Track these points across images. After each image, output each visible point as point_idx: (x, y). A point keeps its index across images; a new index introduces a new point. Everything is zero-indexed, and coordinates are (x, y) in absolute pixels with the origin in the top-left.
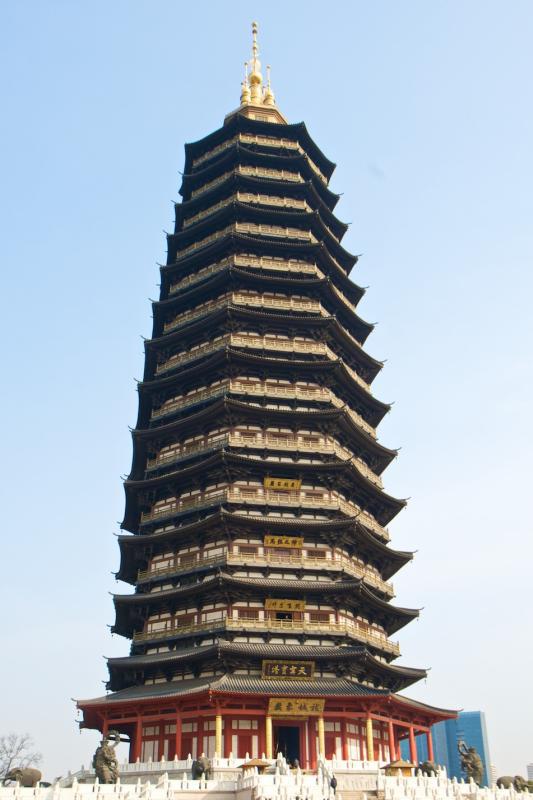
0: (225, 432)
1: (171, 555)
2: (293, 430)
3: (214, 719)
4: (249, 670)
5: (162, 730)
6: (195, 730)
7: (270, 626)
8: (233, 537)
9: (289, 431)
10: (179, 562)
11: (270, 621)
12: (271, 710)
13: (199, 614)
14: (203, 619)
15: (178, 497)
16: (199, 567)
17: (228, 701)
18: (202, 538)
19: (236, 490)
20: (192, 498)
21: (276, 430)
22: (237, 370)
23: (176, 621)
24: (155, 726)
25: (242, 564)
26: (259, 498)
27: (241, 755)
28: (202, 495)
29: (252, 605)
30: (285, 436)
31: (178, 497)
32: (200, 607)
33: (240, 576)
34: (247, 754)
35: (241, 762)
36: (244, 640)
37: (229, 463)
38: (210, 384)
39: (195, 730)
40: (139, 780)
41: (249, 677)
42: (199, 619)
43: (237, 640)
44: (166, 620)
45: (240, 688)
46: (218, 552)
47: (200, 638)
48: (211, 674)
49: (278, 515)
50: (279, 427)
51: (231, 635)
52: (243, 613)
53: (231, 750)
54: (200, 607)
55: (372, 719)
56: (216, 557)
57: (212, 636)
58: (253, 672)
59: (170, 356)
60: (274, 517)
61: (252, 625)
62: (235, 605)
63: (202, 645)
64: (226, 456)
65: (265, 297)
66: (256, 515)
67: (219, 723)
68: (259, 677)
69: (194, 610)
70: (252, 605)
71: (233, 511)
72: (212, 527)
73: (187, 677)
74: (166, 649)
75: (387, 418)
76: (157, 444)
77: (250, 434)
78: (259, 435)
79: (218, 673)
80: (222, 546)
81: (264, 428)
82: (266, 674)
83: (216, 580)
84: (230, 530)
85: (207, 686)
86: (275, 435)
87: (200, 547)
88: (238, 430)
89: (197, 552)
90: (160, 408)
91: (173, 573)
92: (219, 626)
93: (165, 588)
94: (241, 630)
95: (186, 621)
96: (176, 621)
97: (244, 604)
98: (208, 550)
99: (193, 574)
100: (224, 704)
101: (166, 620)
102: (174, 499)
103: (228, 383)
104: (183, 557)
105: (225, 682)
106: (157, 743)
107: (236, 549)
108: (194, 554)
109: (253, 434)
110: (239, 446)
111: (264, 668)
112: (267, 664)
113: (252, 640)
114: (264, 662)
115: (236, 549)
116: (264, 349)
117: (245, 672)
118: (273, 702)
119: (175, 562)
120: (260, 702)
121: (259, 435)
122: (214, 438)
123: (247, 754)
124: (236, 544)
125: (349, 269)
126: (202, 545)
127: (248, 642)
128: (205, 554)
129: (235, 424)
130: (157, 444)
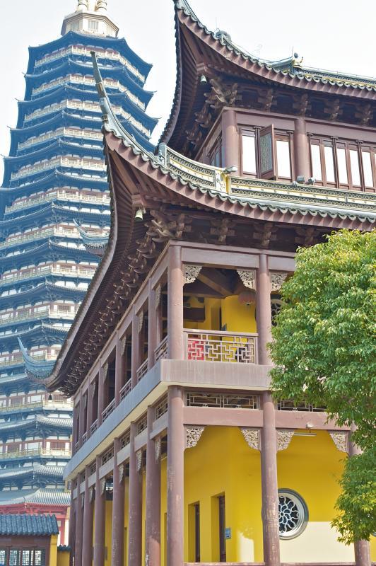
0: (49, 265)
1: (12, 309)
2: (101, 226)
4: (56, 485)
7: (79, 273)
8: (62, 185)
9: (97, 227)
10: (10, 403)
11: (79, 270)
13: (23, 443)
14: (29, 401)
15: (11, 351)
16: (23, 409)
17: (38, 509)
18: (34, 299)
19: (58, 266)
20: (28, 271)
21: (87, 264)
22: (60, 218)
23: (17, 313)
26: (72, 273)
28: (36, 268)
29: (61, 438)
30: (95, 194)
31: (11, 351)
32: (27, 391)
33: (60, 284)
37: (52, 291)
38: (41, 226)
41: (56, 490)
42: (26, 400)
43: (48, 464)
44: (10, 312)
45: (48, 500)
46: (44, 308)
47: (26, 414)
48: (30, 487)
49: (90, 176)
50: (90, 223)
51: (44, 461)
54: (24, 438)
56: (42, 313)
57: (34, 413)
58: (59, 487)
59: (9, 234)
60: (86, 177)
62: (48, 439)
63: (28, 418)
64: (61, 144)
65: (85, 131)
66: (75, 175)
68: (63, 490)
69: (20, 440)
71: (55, 281)
72: (44, 253)
73: (13, 489)
74: (6, 375)
75: (153, 99)
76: (6, 232)
77: (71, 192)
78: (74, 267)
79: (35, 487)
80: (47, 305)
81: (78, 262)
83: (40, 329)
84: (48, 338)
85: (22, 498)
86: (88, 194)
89: (30, 308)
90: (17, 172)
91: (12, 322)
92: (36, 454)
93: (8, 333)
95: (13, 448)
96: (7, 447)
97: (55, 438)
98: (33, 351)
99: (26, 324)
101: (10, 312)
102: (8, 353)
103: (60, 158)
104: (20, 311)
107: (56, 307)
108: (21, 398)
109: (70, 266)
110: (56, 318)
113: (62, 416)
115: (56, 307)
116: (83, 110)
117: (54, 487)
119: (14, 315)
121: (74, 267)
122: (42, 268)
124: (56, 304)
125: (142, 86)
126: (27, 391)
128: (35, 310)
129: (57, 259)
130: (6, 232)
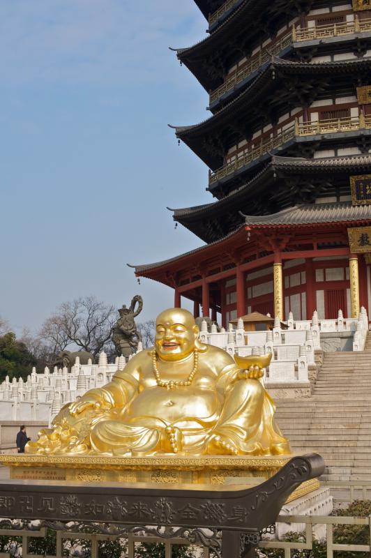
3: (271, 265)
5: (311, 276)
6: (304, 282)
12: (355, 247)
24: (300, 272)
25: (317, 43)
27: (331, 314)
29: (339, 101)
34: (340, 312)
35: (113, 368)
36: (331, 154)
39: (304, 282)
40: (34, 369)
41: (339, 204)
52: (325, 114)
53: (315, 309)
55: (283, 262)
61: (335, 130)
67: (278, 272)
68: (349, 204)
70: (339, 101)
82: (359, 198)
87: (271, 37)
88: (315, 110)
94: (319, 138)
100: (283, 246)
105: (297, 215)
106: (304, 294)
111: (354, 189)
112: (357, 183)
113: (341, 152)
114: (353, 180)
118: (355, 235)
120: (335, 234)
123: (340, 312)
127: (336, 156)
